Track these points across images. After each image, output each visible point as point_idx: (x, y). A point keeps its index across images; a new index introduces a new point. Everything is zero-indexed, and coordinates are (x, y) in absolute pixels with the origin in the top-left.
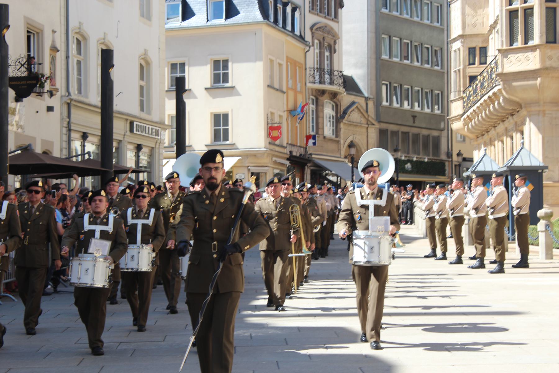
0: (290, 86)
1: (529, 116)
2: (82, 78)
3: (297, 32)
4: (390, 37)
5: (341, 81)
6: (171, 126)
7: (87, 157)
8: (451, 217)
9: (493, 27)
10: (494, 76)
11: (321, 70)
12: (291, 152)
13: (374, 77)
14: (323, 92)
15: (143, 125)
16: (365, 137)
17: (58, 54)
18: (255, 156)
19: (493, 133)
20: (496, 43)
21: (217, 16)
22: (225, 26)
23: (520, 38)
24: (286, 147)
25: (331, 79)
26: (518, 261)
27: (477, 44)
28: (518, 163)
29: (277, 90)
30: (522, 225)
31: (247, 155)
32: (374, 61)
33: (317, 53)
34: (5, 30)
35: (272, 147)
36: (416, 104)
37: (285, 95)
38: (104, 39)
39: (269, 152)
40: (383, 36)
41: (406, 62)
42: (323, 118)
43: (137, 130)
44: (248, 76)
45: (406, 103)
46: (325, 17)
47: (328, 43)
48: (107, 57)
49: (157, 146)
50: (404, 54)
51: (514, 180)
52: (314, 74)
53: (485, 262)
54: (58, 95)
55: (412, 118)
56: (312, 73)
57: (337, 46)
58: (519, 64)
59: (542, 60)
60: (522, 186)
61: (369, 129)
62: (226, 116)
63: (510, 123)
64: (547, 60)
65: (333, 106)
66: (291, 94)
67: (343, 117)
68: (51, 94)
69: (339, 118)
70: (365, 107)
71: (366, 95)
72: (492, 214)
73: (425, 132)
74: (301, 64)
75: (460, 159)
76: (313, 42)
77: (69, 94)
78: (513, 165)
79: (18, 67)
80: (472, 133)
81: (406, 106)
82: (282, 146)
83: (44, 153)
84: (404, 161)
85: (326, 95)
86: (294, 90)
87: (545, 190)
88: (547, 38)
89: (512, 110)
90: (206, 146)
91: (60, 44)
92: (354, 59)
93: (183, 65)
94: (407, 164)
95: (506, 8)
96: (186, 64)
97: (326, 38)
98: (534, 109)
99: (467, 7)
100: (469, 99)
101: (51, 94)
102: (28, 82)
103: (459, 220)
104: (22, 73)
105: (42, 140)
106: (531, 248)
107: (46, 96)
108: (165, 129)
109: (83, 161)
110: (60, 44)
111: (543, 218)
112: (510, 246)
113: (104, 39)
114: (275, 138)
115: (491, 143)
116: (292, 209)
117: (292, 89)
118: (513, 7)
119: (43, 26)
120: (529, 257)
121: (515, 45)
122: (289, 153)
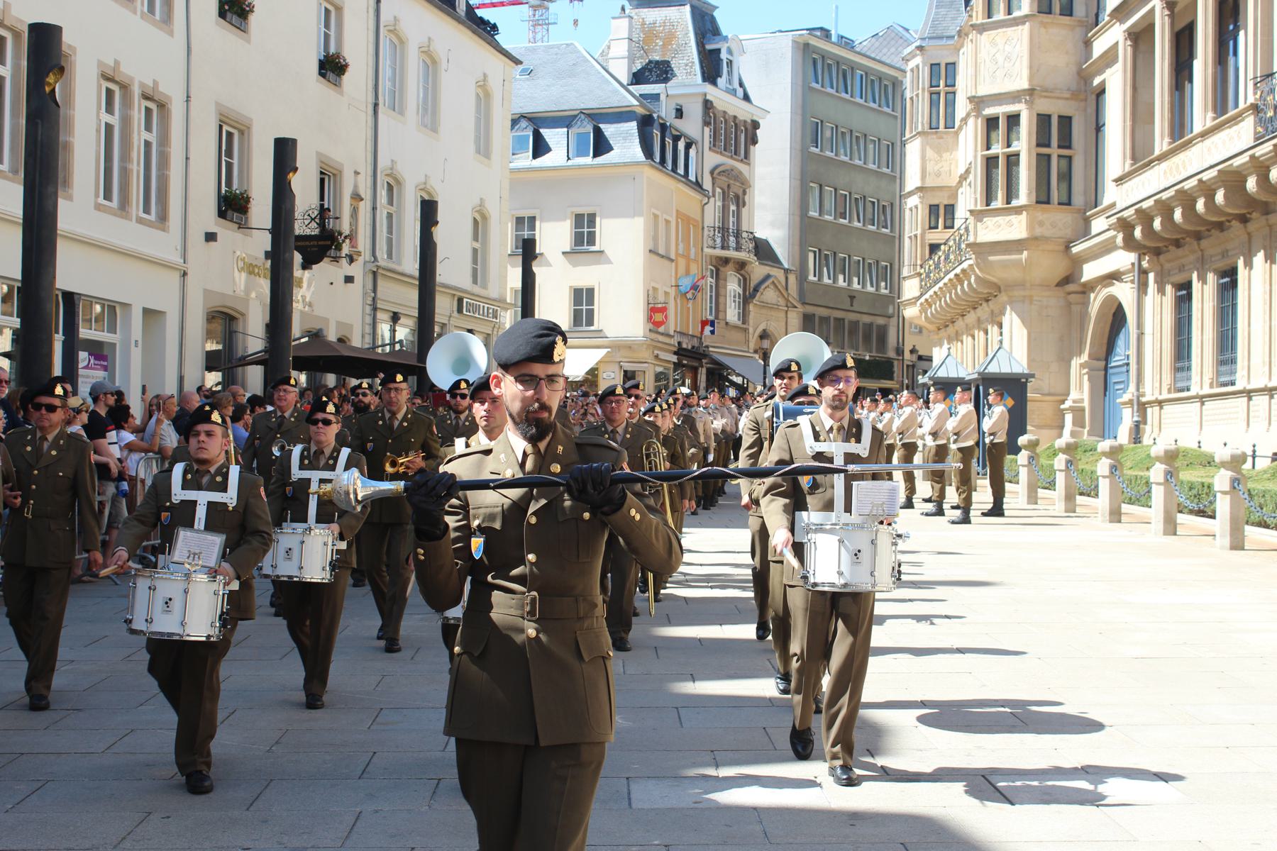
0: (681, 252)
1: (1011, 303)
2: (394, 237)
3: (692, 177)
5: (751, 246)
6: (515, 305)
7: (398, 347)
8: (900, 444)
9: (963, 177)
10: (963, 246)
11: (724, 230)
12: (679, 343)
14: (726, 261)
17: (362, 204)
19: (960, 324)
20: (968, 200)
21: (581, 153)
22: (591, 167)
25: (738, 243)
26: (990, 506)
27: (942, 200)
28: (993, 369)
29: (663, 257)
30: (994, 458)
31: (618, 346)
32: (797, 219)
35: (654, 336)
36: (855, 280)
39: (649, 342)
44: (623, 237)
45: (841, 277)
47: (735, 194)
48: (429, 211)
50: (841, 210)
51: (987, 394)
53: (945, 506)
54: (361, 260)
57: (747, 198)
59: (1030, 227)
60: (997, 404)
62: (590, 292)
63: (984, 311)
67: (753, 296)
68: (351, 259)
69: (748, 297)
72: (955, 442)
73: (867, 319)
75: (914, 358)
76: (714, 191)
77: (376, 259)
80: (931, 323)
81: (841, 282)
83: (340, 340)
85: (731, 265)
86: (687, 257)
87: (1030, 406)
91: (365, 192)
92: (770, 215)
93: (532, 220)
95: (982, 153)
98: (1018, 293)
100: (928, 276)
101: (351, 259)
103: (910, 449)
104: (313, 229)
105: (338, 322)
106: (1008, 486)
107: (344, 261)
108: (506, 309)
109: (393, 352)
110: (365, 192)
111: (1026, 447)
112: (979, 482)
114: (658, 324)
115: (957, 337)
116: (647, 449)
117: (683, 256)
118: (992, 151)
120: (1005, 500)
121: (994, 205)
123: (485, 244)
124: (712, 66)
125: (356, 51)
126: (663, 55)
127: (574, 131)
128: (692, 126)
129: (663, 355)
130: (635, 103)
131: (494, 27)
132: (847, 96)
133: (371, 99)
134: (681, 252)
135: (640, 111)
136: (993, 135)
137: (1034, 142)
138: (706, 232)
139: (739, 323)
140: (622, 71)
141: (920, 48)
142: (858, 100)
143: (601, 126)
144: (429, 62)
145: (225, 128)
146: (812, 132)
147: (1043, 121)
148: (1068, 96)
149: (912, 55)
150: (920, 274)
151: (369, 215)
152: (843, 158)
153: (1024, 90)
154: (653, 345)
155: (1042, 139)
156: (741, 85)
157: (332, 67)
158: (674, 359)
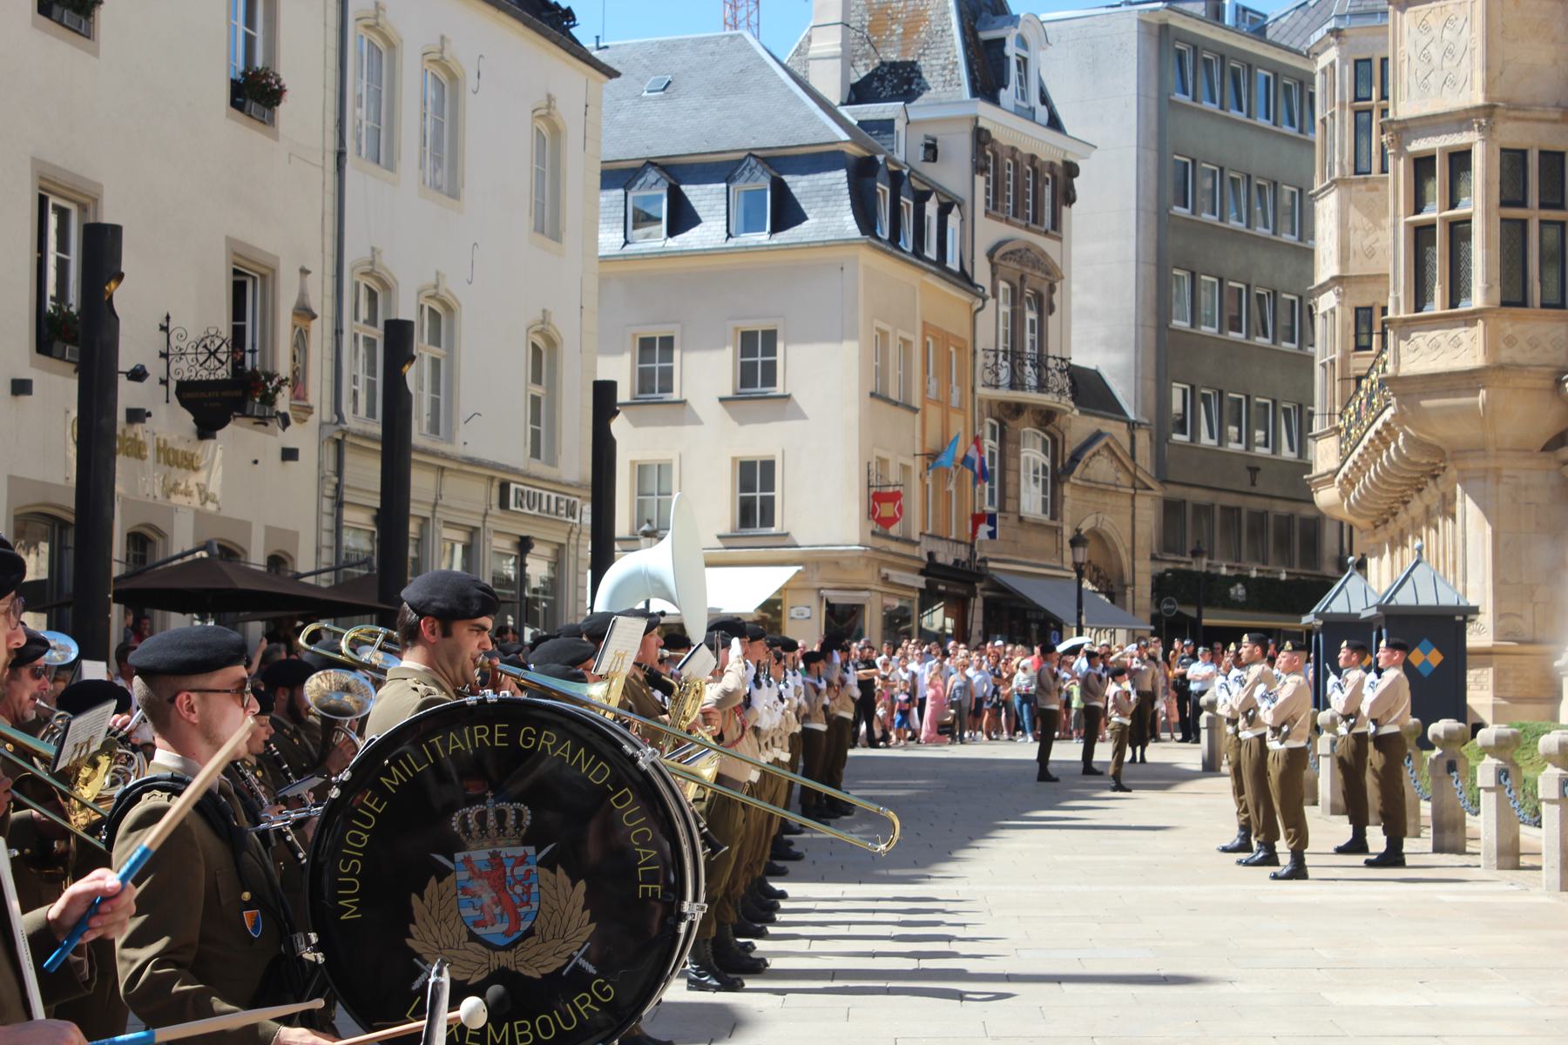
0: (932, 394)
1: (1463, 481)
3: (953, 263)
4: (1193, 275)
11: (1015, 355)
12: (931, 555)
13: (1151, 374)
14: (1017, 409)
15: (526, 489)
16: (1128, 518)
17: (315, 324)
18: (837, 563)
21: (751, 225)
22: (769, 249)
23: (1439, 292)
24: (917, 544)
28: (1405, 598)
29: (896, 404)
31: (814, 562)
32: (1151, 333)
33: (1005, 314)
34: (113, 285)
37: (918, 416)
38: (436, 287)
39: (871, 554)
40: (1176, 272)
41: (1233, 335)
42: (1018, 471)
43: (519, 503)
44: (825, 376)
46: (1027, 227)
47: (1035, 289)
49: (573, 541)
52: (996, 363)
54: (314, 419)
55: (1248, 473)
56: (991, 361)
57: (1056, 298)
58: (1435, 354)
59: (1490, 346)
61: (1137, 499)
62: (768, 466)
63: (1431, 494)
64: (1503, 346)
65: (1045, 442)
66: (934, 414)
67: (1069, 470)
70: (1127, 447)
71: (1132, 416)
74: (963, 341)
77: (341, 418)
78: (1393, 603)
79: (202, 358)
82: (908, 541)
84: (1226, 577)
85: (1026, 415)
86: (944, 403)
88: (1503, 293)
89: (1428, 464)
90: (720, 537)
91: (321, 302)
92: (1099, 327)
94: (1233, 585)
96: (676, 342)
97: (1029, 278)
98: (1473, 464)
99: (1352, 210)
102: (224, 394)
105: (268, 528)
110: (321, 302)
113: (436, 287)
114: (886, 522)
117: (937, 402)
119: (277, 258)
122: (925, 558)
123: (553, 388)
124: (989, 70)
125: (302, 64)
126: (905, 51)
127: (739, 186)
128: (954, 173)
129: (896, 576)
130: (844, 136)
131: (568, 14)
132: (1241, 116)
133: (331, 144)
134: (932, 394)
135: (854, 150)
136: (1429, 187)
137: (1496, 199)
138: (980, 359)
139: (1046, 518)
140: (831, 86)
141: (1336, 33)
142: (1261, 122)
143: (787, 178)
144: (443, 77)
145: (52, 200)
146: (1174, 180)
147: (1513, 161)
148: (1557, 115)
149: (1323, 46)
150: (1338, 430)
151: (329, 344)
152: (1233, 223)
153: (1477, 108)
154: (876, 557)
155: (1511, 191)
156: (1044, 99)
157: (255, 93)
158: (920, 582)
